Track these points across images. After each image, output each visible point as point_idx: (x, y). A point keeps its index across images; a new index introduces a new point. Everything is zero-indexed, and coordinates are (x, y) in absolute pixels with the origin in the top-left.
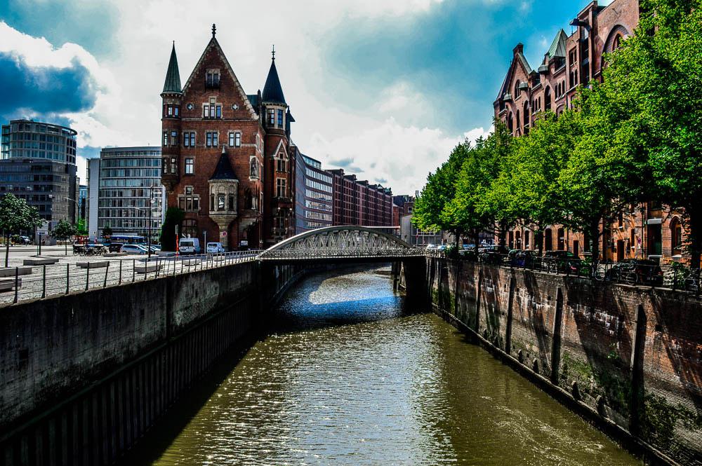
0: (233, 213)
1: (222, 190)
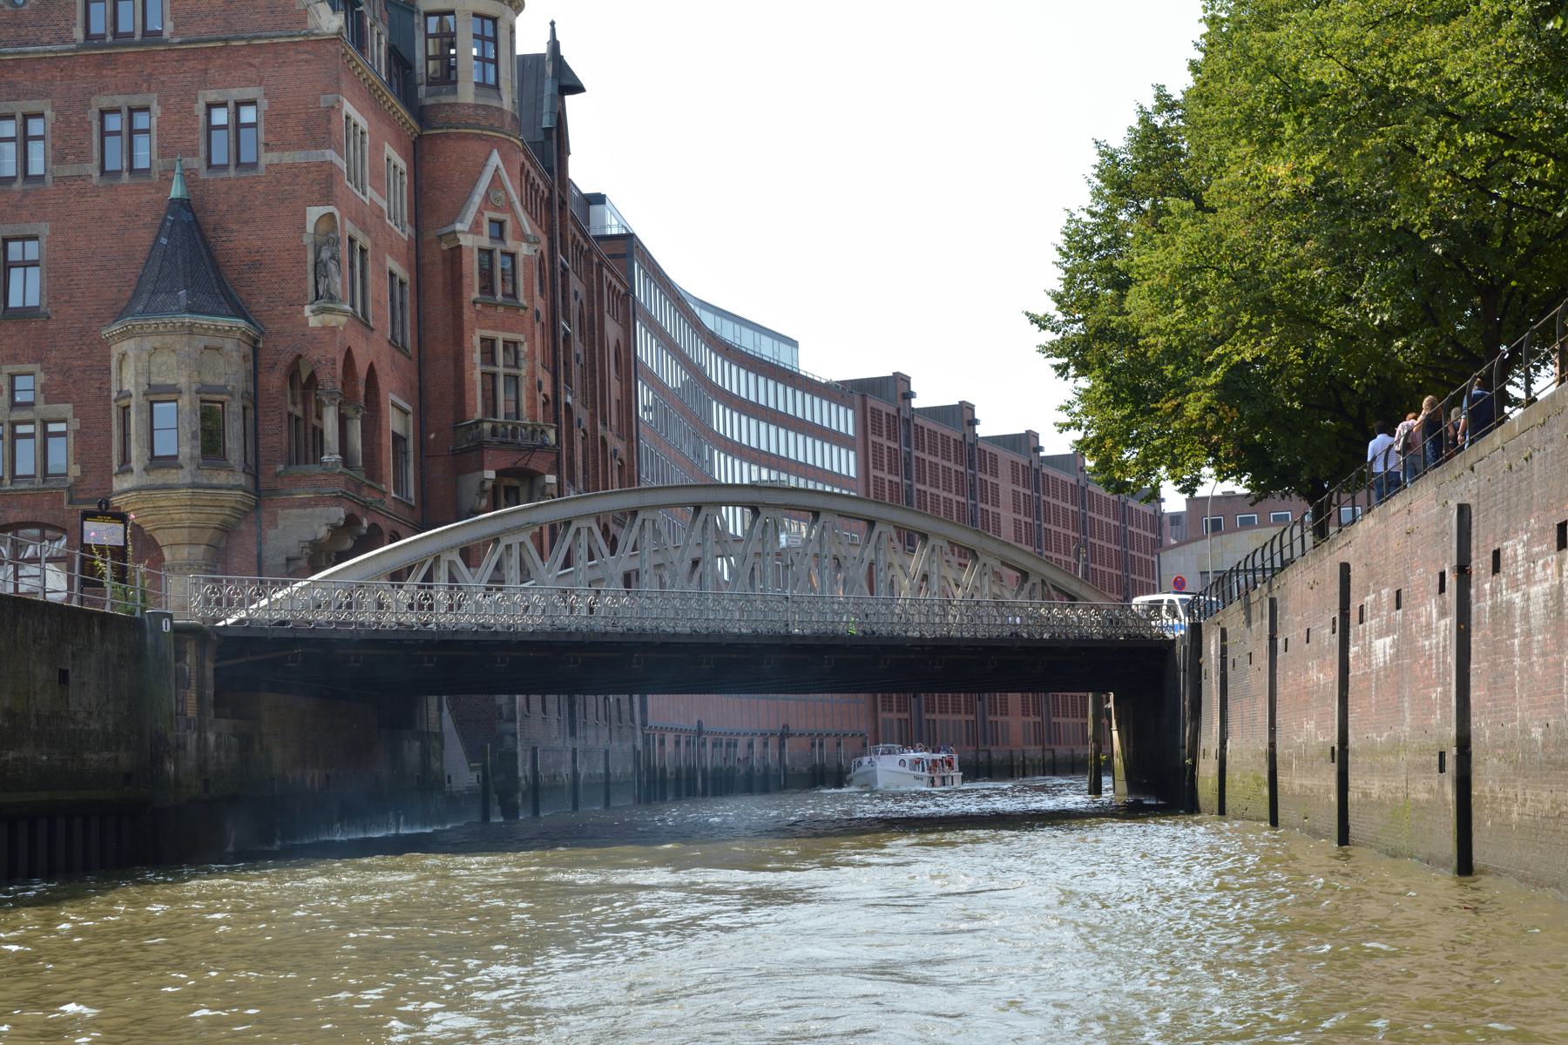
0: (222, 478)
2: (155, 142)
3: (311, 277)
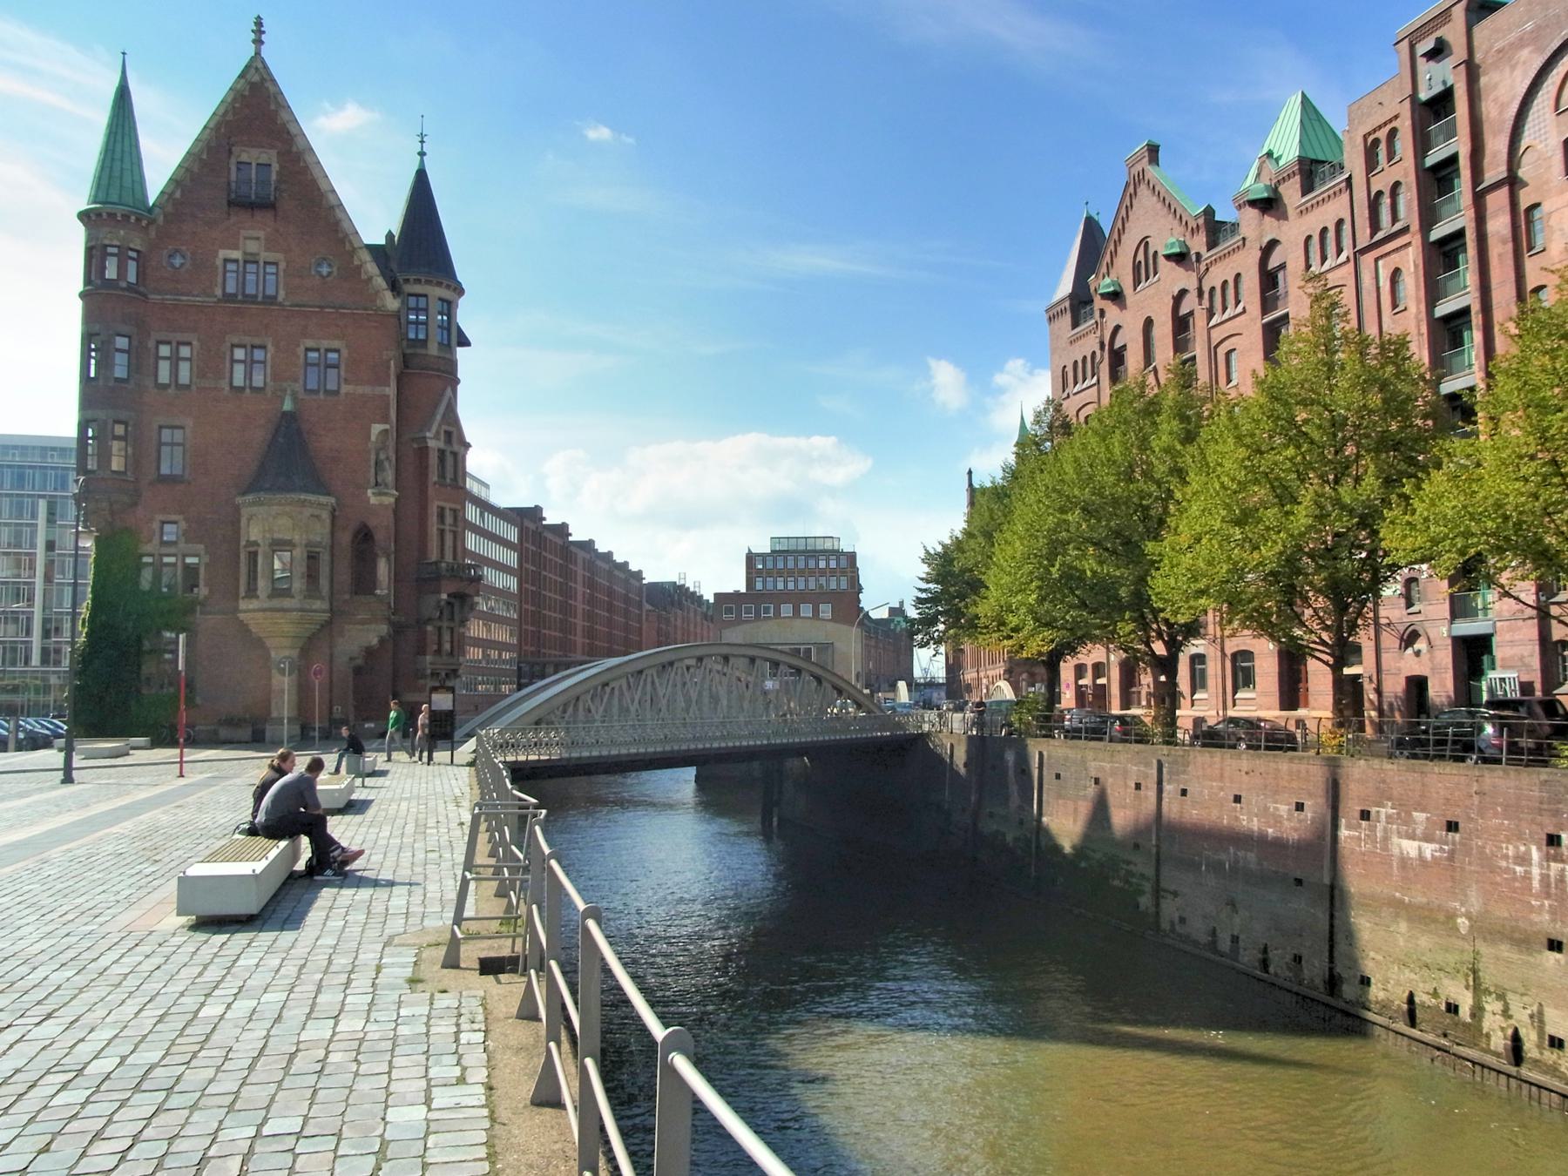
0: (318, 605)
1: (283, 528)
2: (269, 371)
3: (373, 470)
